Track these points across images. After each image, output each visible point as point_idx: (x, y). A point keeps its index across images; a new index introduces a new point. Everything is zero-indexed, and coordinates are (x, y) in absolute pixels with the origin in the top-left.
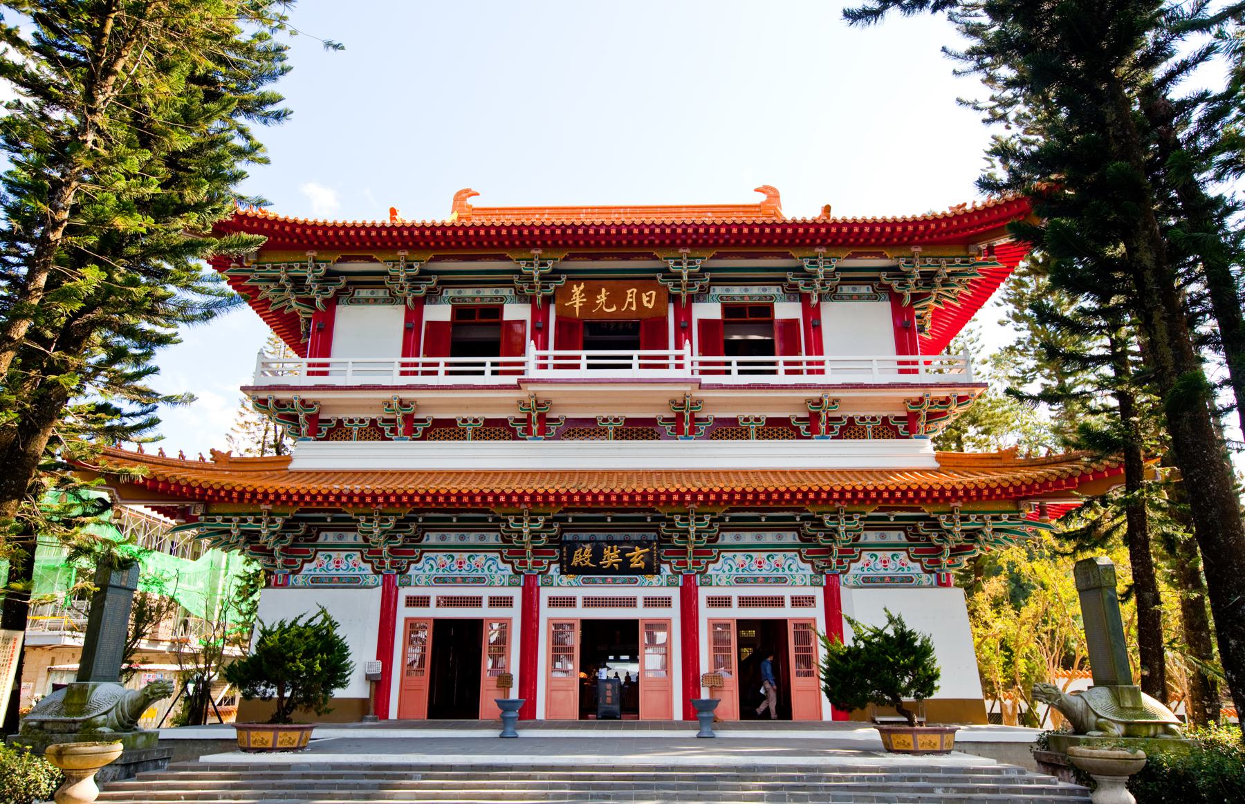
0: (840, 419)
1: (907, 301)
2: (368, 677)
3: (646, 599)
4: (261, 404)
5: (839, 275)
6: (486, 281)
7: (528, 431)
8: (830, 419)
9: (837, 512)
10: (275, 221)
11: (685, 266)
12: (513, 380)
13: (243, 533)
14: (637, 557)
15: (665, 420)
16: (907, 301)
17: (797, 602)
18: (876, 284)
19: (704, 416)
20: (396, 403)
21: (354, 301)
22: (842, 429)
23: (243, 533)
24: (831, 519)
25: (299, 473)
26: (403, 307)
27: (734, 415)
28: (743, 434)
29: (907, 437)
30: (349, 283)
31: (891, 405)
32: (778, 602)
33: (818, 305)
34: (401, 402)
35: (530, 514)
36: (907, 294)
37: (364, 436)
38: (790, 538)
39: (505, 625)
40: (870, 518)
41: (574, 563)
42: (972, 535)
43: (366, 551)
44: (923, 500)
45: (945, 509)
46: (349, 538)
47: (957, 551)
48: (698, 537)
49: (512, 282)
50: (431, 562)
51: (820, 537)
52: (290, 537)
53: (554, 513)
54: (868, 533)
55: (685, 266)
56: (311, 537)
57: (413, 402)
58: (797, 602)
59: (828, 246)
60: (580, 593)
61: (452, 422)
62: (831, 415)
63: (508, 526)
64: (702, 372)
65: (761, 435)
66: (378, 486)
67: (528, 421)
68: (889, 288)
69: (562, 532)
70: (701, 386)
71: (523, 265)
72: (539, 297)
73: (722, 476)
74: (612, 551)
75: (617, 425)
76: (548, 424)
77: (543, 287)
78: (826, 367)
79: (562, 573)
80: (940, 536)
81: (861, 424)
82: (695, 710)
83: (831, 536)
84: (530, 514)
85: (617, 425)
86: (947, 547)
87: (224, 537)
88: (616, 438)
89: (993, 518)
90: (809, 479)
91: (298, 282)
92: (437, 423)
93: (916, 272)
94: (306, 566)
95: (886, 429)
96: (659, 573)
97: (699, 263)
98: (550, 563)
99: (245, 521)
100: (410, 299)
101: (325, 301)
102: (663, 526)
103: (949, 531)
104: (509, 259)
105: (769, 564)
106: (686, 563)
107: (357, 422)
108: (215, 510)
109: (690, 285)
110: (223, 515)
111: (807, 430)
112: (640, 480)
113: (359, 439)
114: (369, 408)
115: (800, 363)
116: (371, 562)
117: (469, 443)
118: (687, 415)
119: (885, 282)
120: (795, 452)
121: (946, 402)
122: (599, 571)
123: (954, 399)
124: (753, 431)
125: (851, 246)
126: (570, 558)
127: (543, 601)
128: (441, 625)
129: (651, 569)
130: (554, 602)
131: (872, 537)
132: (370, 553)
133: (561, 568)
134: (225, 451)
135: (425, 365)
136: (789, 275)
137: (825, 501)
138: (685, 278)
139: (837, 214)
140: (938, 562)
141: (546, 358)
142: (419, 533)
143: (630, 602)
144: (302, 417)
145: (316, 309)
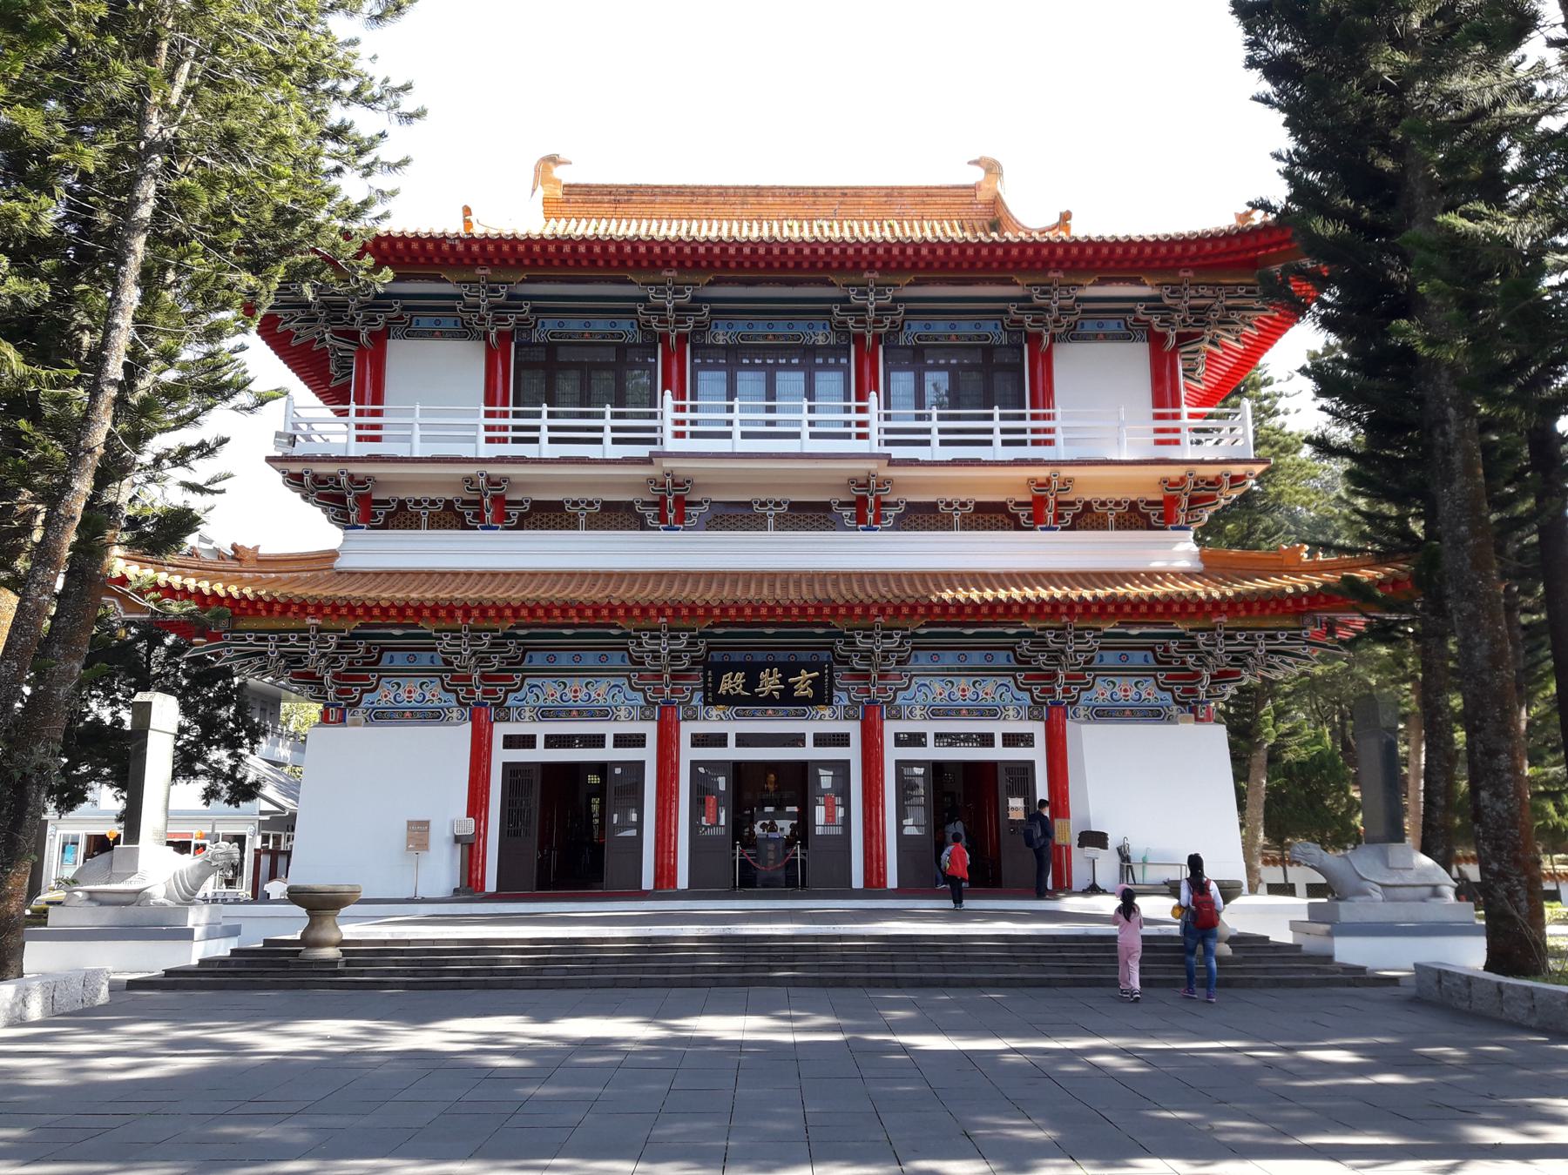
1: (1172, 342)
3: (811, 735)
4: (295, 480)
6: (588, 310)
7: (479, 516)
8: (1059, 504)
9: (1064, 628)
12: (642, 451)
14: (803, 683)
15: (842, 504)
16: (1172, 342)
17: (622, 741)
19: (892, 499)
20: (482, 480)
21: (410, 335)
22: (1076, 517)
25: (352, 574)
26: (483, 343)
27: (932, 499)
28: (945, 524)
31: (1144, 485)
33: (1050, 348)
35: (670, 630)
36: (1172, 334)
37: (436, 523)
39: (842, 767)
40: (1107, 635)
41: (722, 690)
45: (1206, 625)
46: (424, 659)
47: (1221, 677)
48: (885, 658)
49: (635, 311)
53: (701, 627)
54: (1104, 653)
56: (372, 663)
59: (1067, 271)
60: (732, 728)
61: (559, 506)
62: (1061, 498)
63: (640, 644)
64: (888, 443)
65: (969, 524)
66: (659, 594)
67: (661, 503)
71: (1035, 293)
72: (673, 336)
76: (688, 510)
77: (677, 322)
78: (1059, 437)
79: (706, 703)
80: (1198, 659)
84: (670, 630)
85: (434, 509)
86: (1206, 673)
87: (257, 662)
88: (963, 529)
89: (1268, 637)
92: (538, 506)
98: (693, 691)
100: (493, 334)
101: (372, 335)
102: (839, 645)
104: (832, 284)
106: (868, 691)
108: (243, 625)
110: (255, 631)
114: (444, 484)
117: (424, 533)
119: (1143, 318)
120: (446, 546)
122: (755, 700)
123: (1227, 479)
125: (1097, 270)
127: (498, 742)
129: (821, 696)
130: (699, 741)
131: (1111, 658)
132: (455, 680)
133: (706, 697)
136: (1140, 308)
138: (872, 315)
141: (682, 423)
143: (797, 740)
144: (350, 499)
145: (360, 345)
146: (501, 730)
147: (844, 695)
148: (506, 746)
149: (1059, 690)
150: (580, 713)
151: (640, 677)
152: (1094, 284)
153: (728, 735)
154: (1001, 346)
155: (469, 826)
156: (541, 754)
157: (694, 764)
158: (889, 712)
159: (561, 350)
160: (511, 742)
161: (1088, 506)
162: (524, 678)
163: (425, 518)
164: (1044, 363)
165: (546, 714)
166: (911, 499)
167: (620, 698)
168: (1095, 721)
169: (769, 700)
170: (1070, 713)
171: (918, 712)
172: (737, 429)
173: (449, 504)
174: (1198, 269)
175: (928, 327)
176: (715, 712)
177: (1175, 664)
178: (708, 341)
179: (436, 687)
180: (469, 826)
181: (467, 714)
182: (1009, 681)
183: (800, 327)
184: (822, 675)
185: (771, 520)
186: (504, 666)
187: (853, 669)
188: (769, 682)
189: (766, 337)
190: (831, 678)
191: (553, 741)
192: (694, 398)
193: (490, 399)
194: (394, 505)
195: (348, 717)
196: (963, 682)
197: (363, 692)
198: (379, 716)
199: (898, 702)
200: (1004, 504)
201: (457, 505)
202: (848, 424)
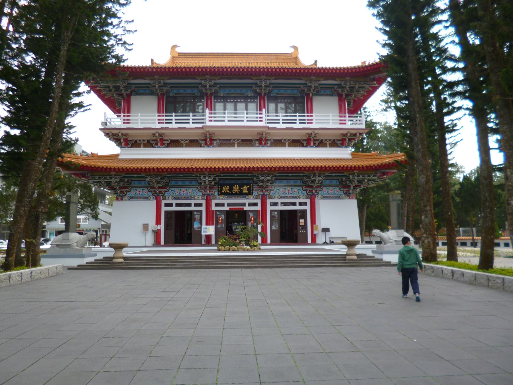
0: (318, 140)
2: (153, 231)
3: (249, 203)
8: (314, 140)
11: (263, 83)
12: (200, 125)
13: (105, 182)
14: (245, 189)
17: (196, 205)
20: (157, 134)
23: (105, 182)
27: (280, 138)
30: (136, 87)
32: (189, 205)
34: (159, 134)
36: (344, 95)
38: (299, 182)
40: (327, 176)
41: (223, 191)
42: (360, 182)
43: (149, 188)
46: (143, 183)
47: (356, 187)
48: (267, 182)
49: (198, 87)
51: (309, 182)
52: (122, 184)
55: (263, 83)
57: (163, 134)
58: (196, 205)
60: (226, 202)
65: (187, 146)
67: (206, 140)
68: (338, 91)
69: (219, 180)
70: (269, 128)
75: (144, 142)
76: (213, 142)
77: (210, 90)
78: (314, 122)
79: (219, 195)
81: (326, 142)
83: (313, 182)
85: (330, 142)
87: (99, 184)
90: (303, 162)
91: (117, 88)
93: (347, 87)
94: (128, 193)
95: (334, 144)
96: (252, 195)
97: (268, 82)
101: (127, 95)
103: (353, 180)
105: (184, 191)
106: (312, 191)
109: (265, 90)
111: (306, 144)
112: (240, 163)
113: (330, 147)
115: (304, 120)
118: (264, 139)
120: (198, 152)
121: (356, 134)
122: (232, 194)
124: (328, 144)
129: (250, 193)
131: (327, 182)
132: (151, 189)
133: (218, 193)
134: (96, 153)
135: (166, 120)
136: (336, 87)
137: (312, 170)
138: (263, 88)
139: (320, 65)
140: (349, 191)
144: (122, 140)
146: (163, 202)
148: (165, 206)
149: (314, 191)
150: (185, 197)
153: (223, 203)
156: (174, 208)
160: (167, 205)
164: (310, 100)
165: (176, 198)
166: (221, 138)
167: (195, 193)
169: (236, 194)
173: (148, 141)
176: (221, 197)
179: (338, 189)
182: (301, 188)
185: (184, 145)
188: (236, 189)
189: (234, 94)
191: (177, 205)
192: (308, 113)
196: (331, 188)
198: (132, 198)
202: (257, 117)
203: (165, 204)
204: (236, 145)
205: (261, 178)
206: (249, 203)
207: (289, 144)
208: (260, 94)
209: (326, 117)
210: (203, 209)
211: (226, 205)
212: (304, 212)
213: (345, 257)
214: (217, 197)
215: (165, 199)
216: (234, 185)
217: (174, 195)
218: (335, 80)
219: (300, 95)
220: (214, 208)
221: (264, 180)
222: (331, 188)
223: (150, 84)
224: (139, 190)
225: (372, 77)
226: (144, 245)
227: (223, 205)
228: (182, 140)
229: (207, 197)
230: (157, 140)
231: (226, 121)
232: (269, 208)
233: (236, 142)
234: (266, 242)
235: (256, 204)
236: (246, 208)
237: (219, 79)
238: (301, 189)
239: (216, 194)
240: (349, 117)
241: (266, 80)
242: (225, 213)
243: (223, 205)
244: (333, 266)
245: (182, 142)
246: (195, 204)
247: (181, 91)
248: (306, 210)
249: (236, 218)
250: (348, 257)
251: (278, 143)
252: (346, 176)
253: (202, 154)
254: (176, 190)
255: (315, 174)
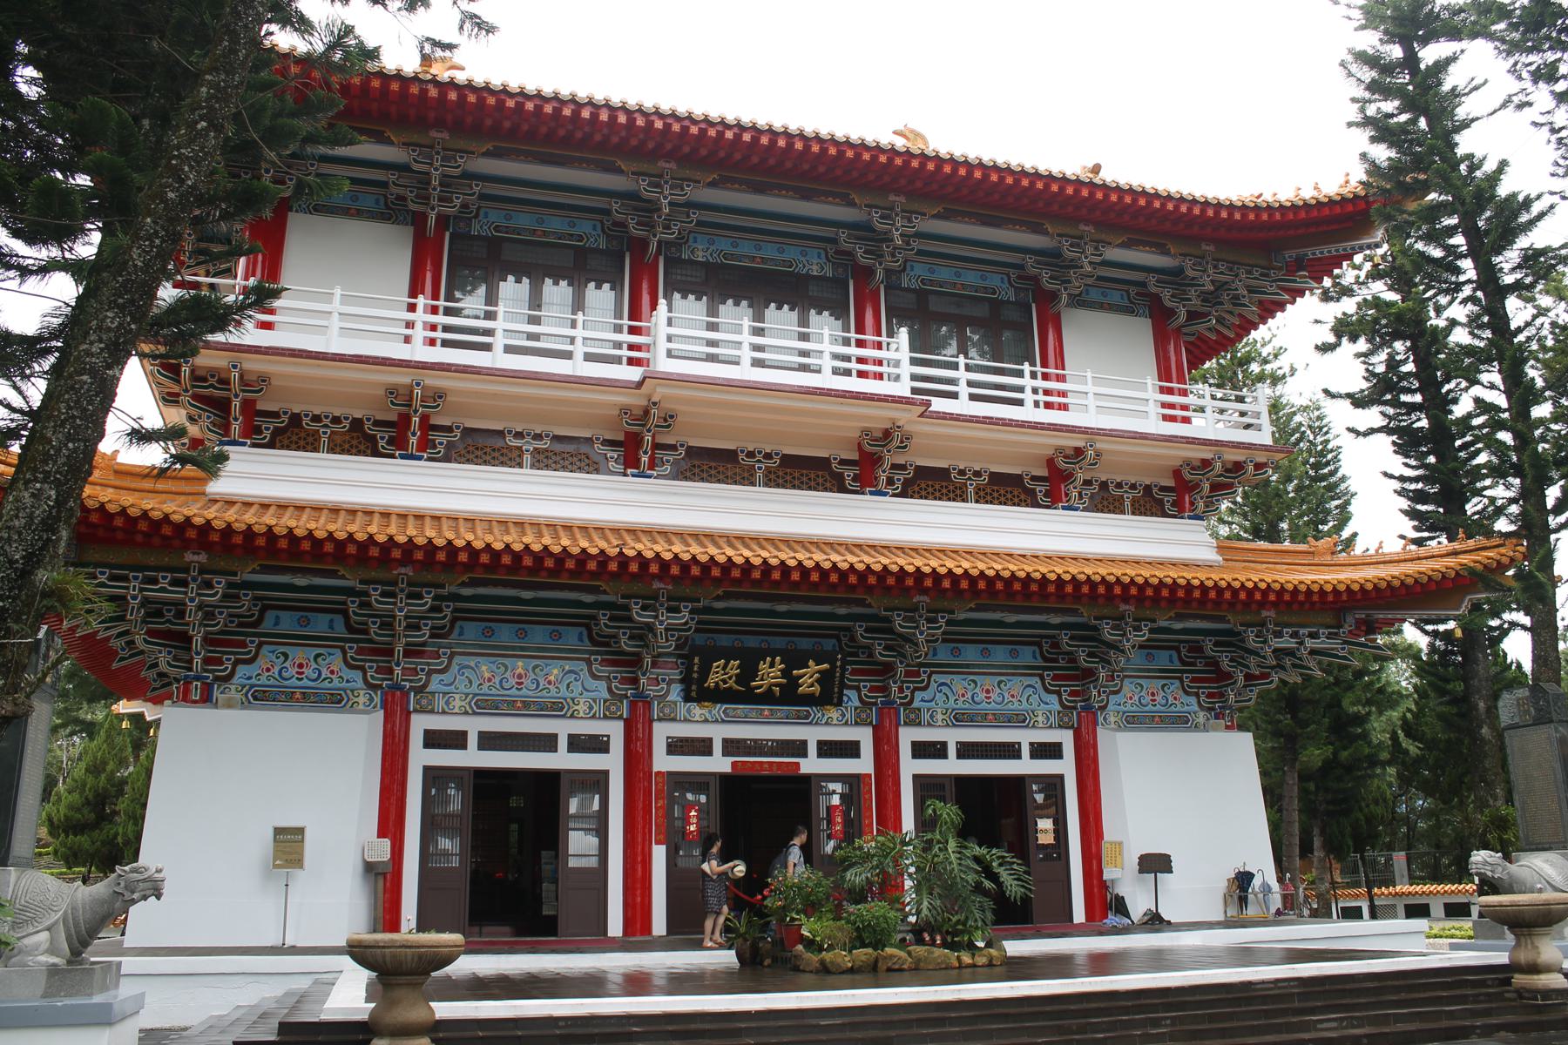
3: (825, 745)
5: (916, 244)
10: (470, 86)
14: (809, 678)
17: (579, 744)
18: (831, 249)
20: (235, 374)
21: (318, 209)
24: (644, 608)
26: (410, 230)
27: (943, 464)
29: (1174, 517)
31: (1154, 468)
32: (547, 743)
37: (339, 447)
39: (1054, 785)
41: (711, 683)
44: (870, 589)
50: (945, 689)
57: (264, 379)
58: (579, 744)
62: (661, 440)
65: (984, 496)
71: (643, 184)
73: (411, 520)
74: (772, 665)
76: (432, 435)
82: (637, 927)
83: (641, 638)
88: (766, 485)
92: (922, 472)
94: (242, 670)
96: (839, 703)
98: (669, 684)
99: (155, 581)
104: (620, 171)
106: (391, 671)
107: (759, 457)
113: (332, 450)
114: (360, 397)
116: (362, 669)
119: (1154, 290)
126: (705, 671)
127: (416, 739)
128: (486, 783)
129: (828, 696)
136: (843, 235)
140: (884, 689)
142: (256, 611)
144: (236, 404)
146: (420, 724)
147: (853, 694)
148: (427, 745)
149: (895, 688)
150: (526, 705)
151: (360, 651)
152: (1123, 245)
153: (704, 740)
154: (1008, 302)
155: (382, 850)
157: (428, 770)
158: (907, 716)
159: (932, 298)
160: (434, 740)
161: (296, 419)
162: (453, 655)
163: (324, 439)
164: (1051, 322)
165: (960, 719)
166: (694, 443)
167: (577, 688)
168: (1126, 729)
169: (767, 698)
170: (1101, 719)
171: (940, 717)
172: (579, 350)
173: (357, 424)
174: (1098, 224)
175: (508, 218)
176: (697, 711)
177: (863, 658)
178: (685, 256)
179: (336, 661)
180: (382, 850)
181: (377, 700)
182: (1035, 681)
183: (791, 253)
184: (833, 666)
186: (232, 627)
187: (371, 641)
188: (770, 674)
189: (753, 259)
190: (842, 676)
191: (489, 741)
192: (1044, 365)
193: (1164, 373)
194: (285, 418)
195: (216, 693)
196: (989, 682)
197: (237, 662)
198: (260, 697)
199: (916, 704)
200: (1019, 477)
201: (367, 425)
202: (618, 345)
203: (915, 745)
204: (527, 458)
205: (640, 617)
206: (825, 745)
207: (978, 490)
208: (639, 246)
209: (1107, 388)
210: (613, 762)
211: (717, 747)
212: (1054, 785)
213: (1508, 982)
214: (682, 709)
215: (916, 723)
216: (761, 655)
217: (474, 689)
218: (1037, 229)
219: (1011, 295)
220: (663, 762)
221: (650, 628)
222: (988, 679)
223: (403, 168)
224: (298, 654)
225: (1290, 255)
226: (272, 940)
227: (701, 747)
228: (316, 418)
229: (633, 706)
230: (401, 422)
231: (579, 356)
232: (910, 768)
233: (529, 445)
234: (647, 927)
235: (850, 750)
236: (811, 765)
237: (713, 184)
238: (1039, 685)
239: (675, 693)
240: (914, 362)
241: (909, 214)
242: (715, 787)
243: (701, 747)
244: (1223, 1033)
245: (314, 426)
246: (820, 744)
247: (524, 220)
248: (1061, 777)
249: (760, 809)
250: (1519, 979)
251: (932, 483)
252: (875, 618)
253: (1161, 542)
254: (959, 683)
255: (915, 609)
